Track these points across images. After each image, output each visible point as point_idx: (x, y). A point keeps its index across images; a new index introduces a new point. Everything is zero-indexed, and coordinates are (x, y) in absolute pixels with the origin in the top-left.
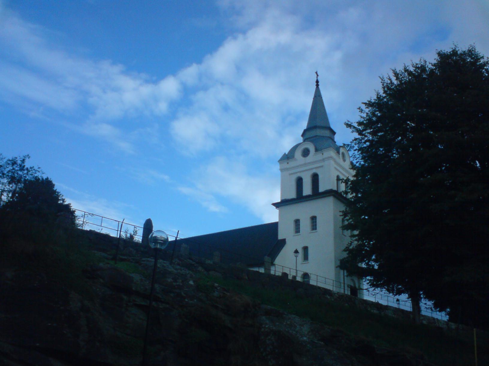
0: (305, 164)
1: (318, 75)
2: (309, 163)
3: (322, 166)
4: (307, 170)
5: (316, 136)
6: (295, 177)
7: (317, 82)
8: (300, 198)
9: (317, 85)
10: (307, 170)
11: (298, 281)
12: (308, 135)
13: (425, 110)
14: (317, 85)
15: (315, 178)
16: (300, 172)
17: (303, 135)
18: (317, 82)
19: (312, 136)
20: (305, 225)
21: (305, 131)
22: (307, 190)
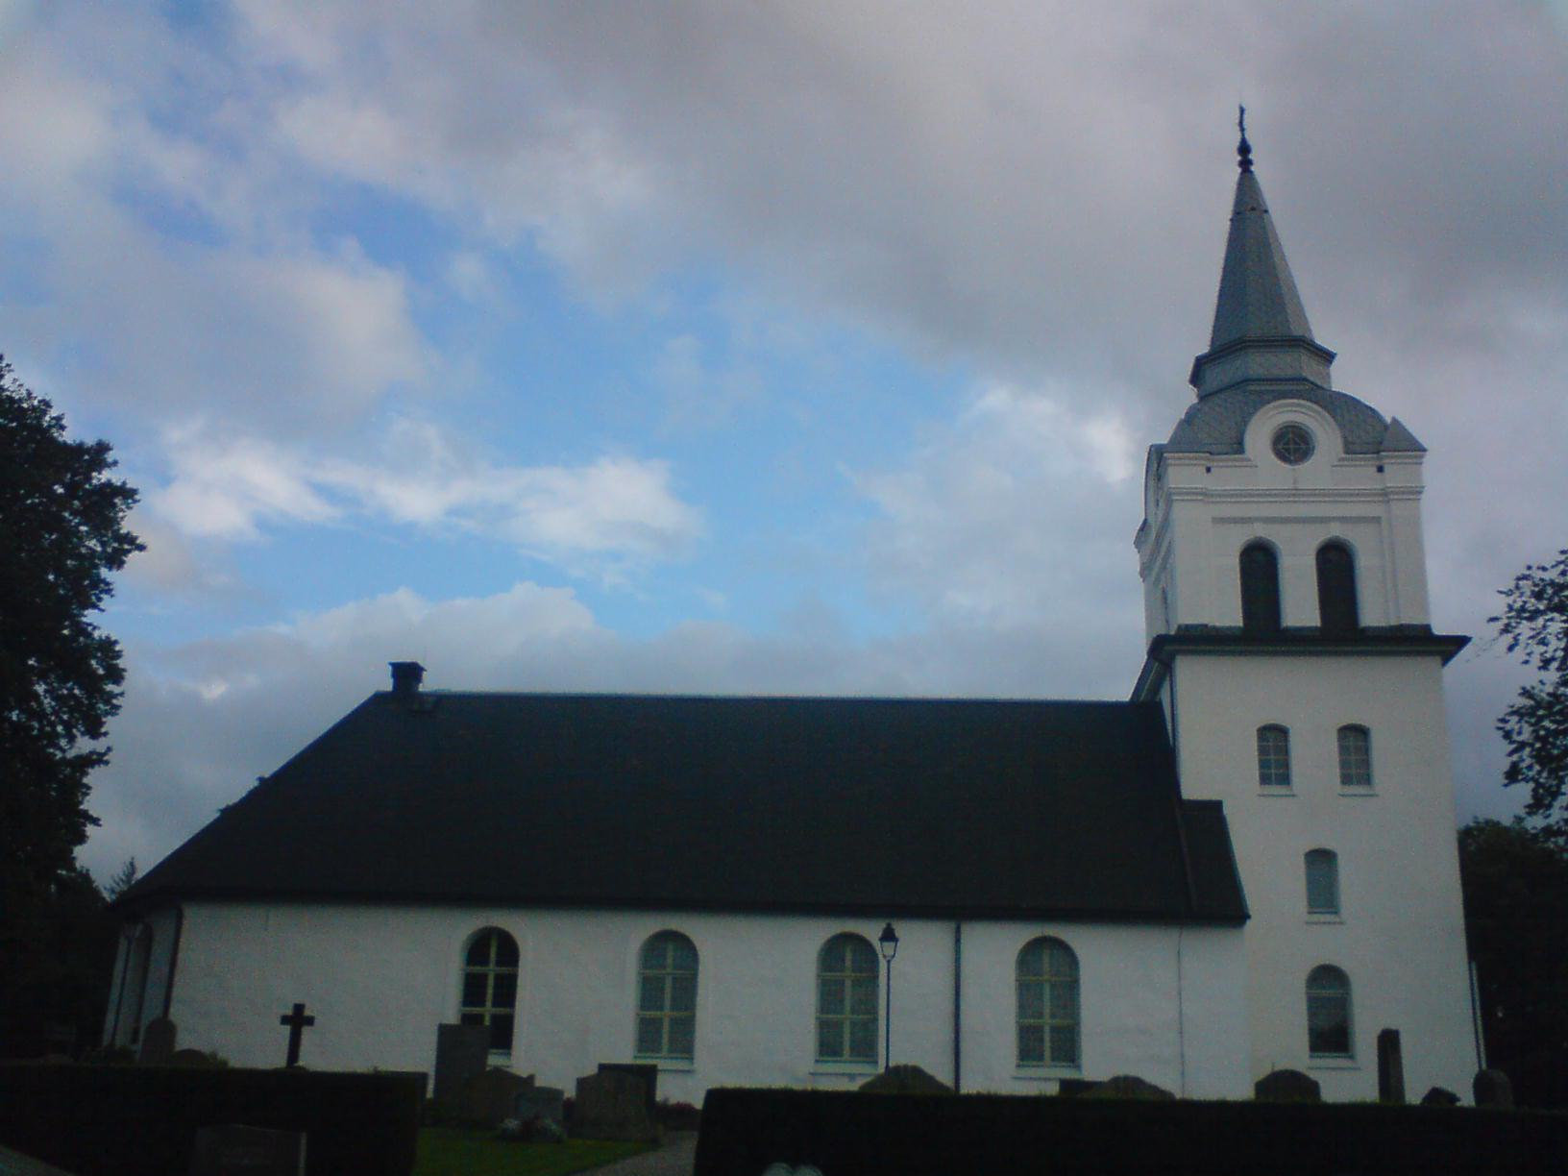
0: (1295, 494)
1: (1241, 124)
2: (1313, 493)
3: (1377, 520)
4: (1235, 521)
5: (1247, 381)
6: (1238, 538)
7: (1244, 149)
8: (1261, 632)
9: (1246, 164)
10: (1235, 521)
11: (1463, 1109)
12: (1215, 377)
13: (51, 577)
14: (1246, 164)
15: (1336, 565)
16: (1267, 520)
17: (1196, 379)
18: (1244, 149)
19: (1276, 372)
20: (1314, 755)
21: (1200, 364)
22: (1300, 605)
